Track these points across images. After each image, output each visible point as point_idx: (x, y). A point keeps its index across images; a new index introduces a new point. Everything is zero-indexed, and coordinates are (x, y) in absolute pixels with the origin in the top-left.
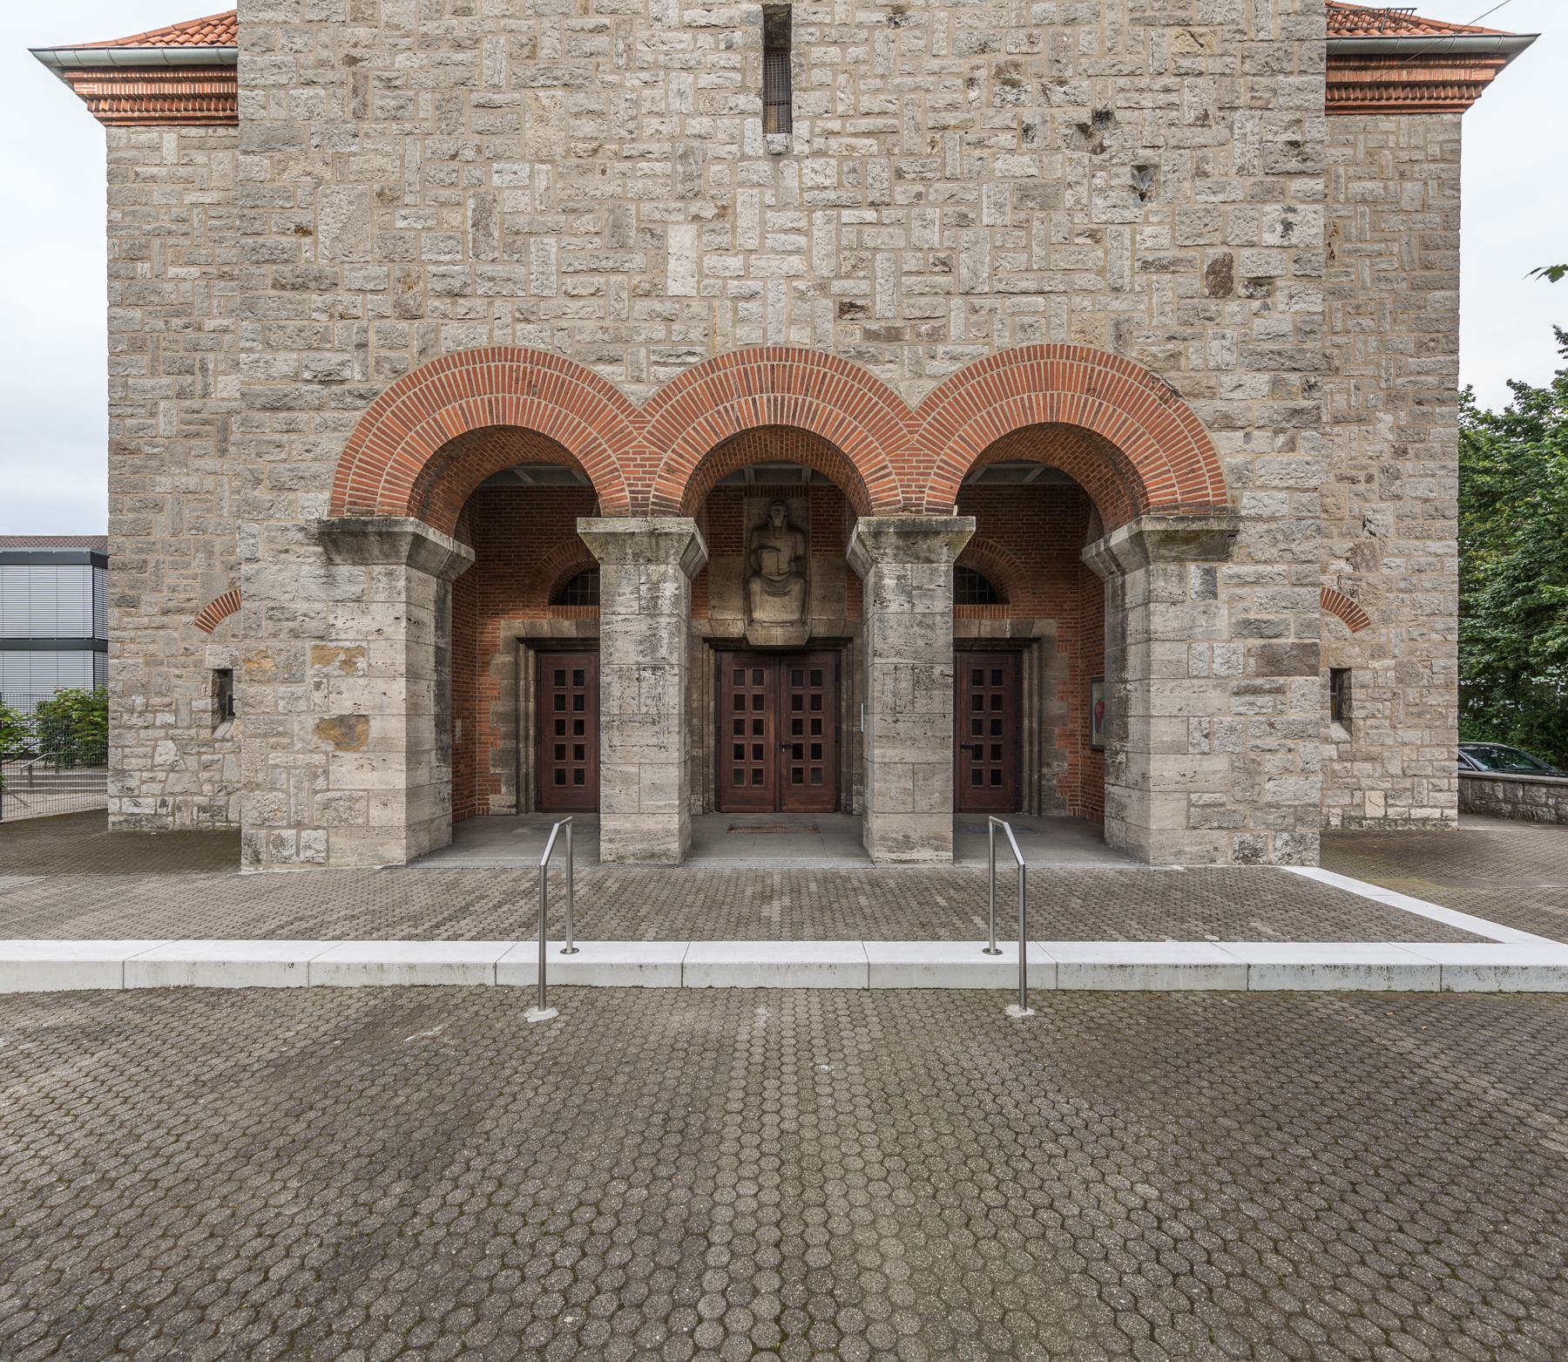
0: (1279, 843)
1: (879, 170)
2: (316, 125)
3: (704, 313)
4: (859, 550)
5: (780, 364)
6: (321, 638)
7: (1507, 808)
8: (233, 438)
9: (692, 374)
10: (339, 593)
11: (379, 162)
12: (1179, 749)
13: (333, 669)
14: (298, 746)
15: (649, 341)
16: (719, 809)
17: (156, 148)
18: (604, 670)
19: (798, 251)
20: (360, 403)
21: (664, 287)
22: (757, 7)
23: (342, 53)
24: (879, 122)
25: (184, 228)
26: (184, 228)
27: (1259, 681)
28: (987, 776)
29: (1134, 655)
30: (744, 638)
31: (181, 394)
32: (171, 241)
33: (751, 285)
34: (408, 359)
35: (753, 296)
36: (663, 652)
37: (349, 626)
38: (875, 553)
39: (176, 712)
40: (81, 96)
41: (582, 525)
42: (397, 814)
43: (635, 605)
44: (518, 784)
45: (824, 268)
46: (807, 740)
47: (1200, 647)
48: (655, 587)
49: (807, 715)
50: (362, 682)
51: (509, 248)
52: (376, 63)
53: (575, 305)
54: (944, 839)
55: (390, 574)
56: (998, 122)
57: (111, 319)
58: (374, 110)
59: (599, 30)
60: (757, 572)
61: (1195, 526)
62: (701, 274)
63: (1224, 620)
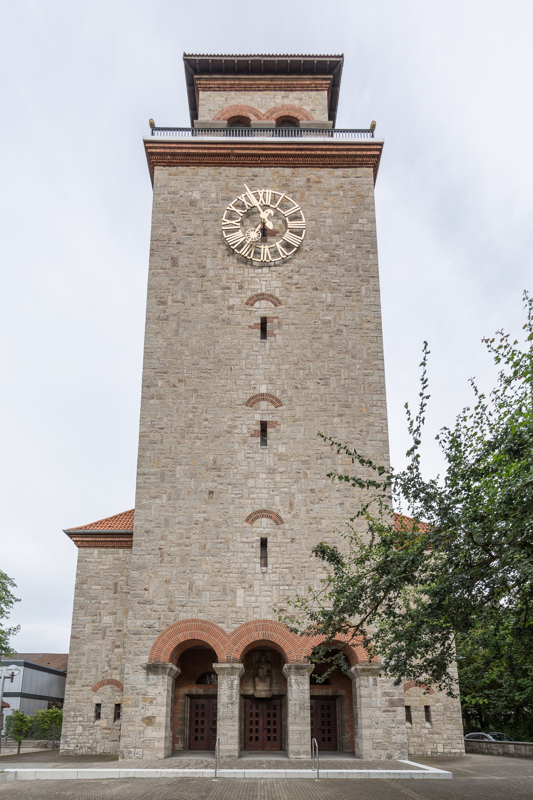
0: (397, 754)
1: (289, 577)
2: (150, 564)
3: (246, 611)
4: (285, 671)
5: (264, 624)
6: (144, 695)
7: (486, 751)
8: (107, 634)
9: (242, 627)
10: (150, 683)
11: (166, 573)
12: (370, 727)
13: (147, 704)
14: (137, 725)
15: (232, 618)
16: (245, 749)
17: (92, 554)
18: (218, 704)
19: (269, 596)
20: (158, 633)
21: (236, 604)
22: (259, 538)
23: (158, 547)
24: (289, 565)
25: (98, 575)
26: (98, 575)
27: (389, 709)
28: (326, 739)
29: (358, 700)
30: (253, 695)
31: (93, 622)
32: (94, 579)
33: (258, 604)
34: (171, 622)
35: (258, 607)
36: (234, 699)
37: (152, 692)
38: (289, 673)
39: (83, 717)
40: (74, 541)
41: (214, 665)
42: (162, 744)
43: (227, 686)
44: (184, 740)
45: (275, 600)
46: (272, 727)
47: (373, 699)
48: (232, 682)
49: (272, 719)
50: (155, 707)
51: (197, 594)
52: (166, 549)
53: (213, 609)
54: (309, 752)
55: (163, 678)
56: (318, 566)
57: (75, 600)
58: (165, 561)
59: (221, 543)
60: (257, 675)
61: (370, 667)
62: (245, 602)
63: (379, 692)
